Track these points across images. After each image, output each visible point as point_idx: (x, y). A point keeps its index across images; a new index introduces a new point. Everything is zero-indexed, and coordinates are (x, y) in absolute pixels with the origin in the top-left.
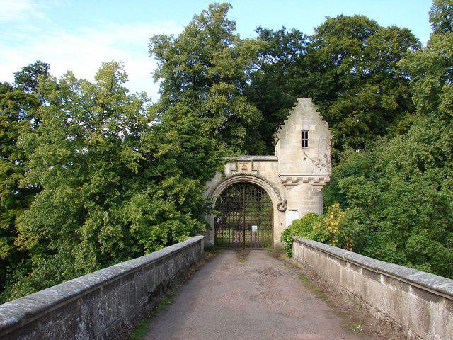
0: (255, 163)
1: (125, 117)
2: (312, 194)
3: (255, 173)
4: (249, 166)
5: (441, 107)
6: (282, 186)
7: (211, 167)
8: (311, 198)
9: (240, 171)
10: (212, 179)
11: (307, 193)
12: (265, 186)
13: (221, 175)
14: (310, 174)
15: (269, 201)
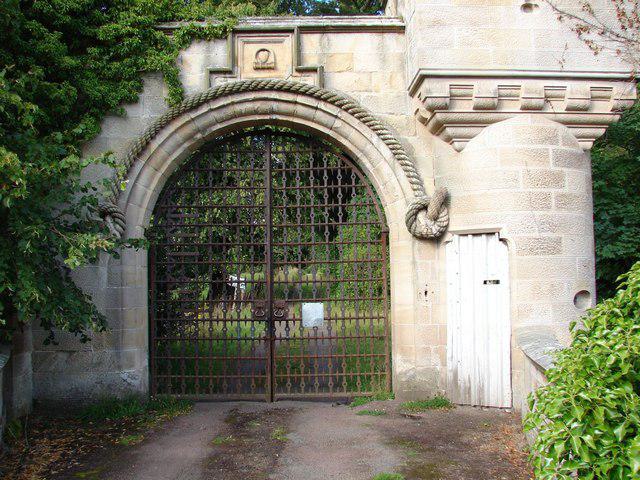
0: (311, 41)
1: (260, 200)
2: (559, 158)
3: (311, 81)
4: (282, 52)
5: (298, 191)
6: (423, 131)
7: (117, 58)
8: (557, 180)
9: (247, 74)
10: (130, 110)
11: (540, 156)
12: (353, 136)
13: (165, 92)
14: (553, 68)
15: (375, 207)
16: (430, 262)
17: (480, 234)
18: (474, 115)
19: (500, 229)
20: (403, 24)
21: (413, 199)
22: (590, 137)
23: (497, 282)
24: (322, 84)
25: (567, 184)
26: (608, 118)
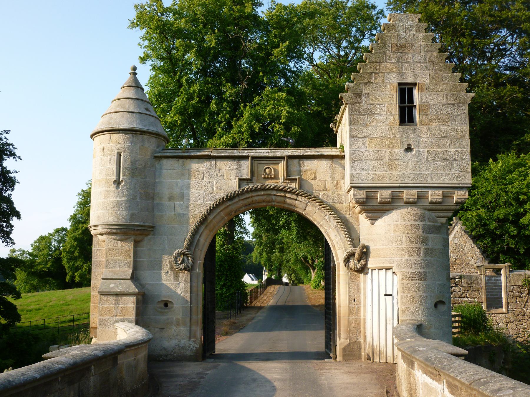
3: (294, 185)
16: (357, 283)
17: (383, 269)
18: (379, 207)
19: (393, 267)
20: (343, 154)
21: (350, 249)
22: (445, 217)
23: (386, 295)
24: (300, 187)
25: (430, 243)
26: (454, 207)
